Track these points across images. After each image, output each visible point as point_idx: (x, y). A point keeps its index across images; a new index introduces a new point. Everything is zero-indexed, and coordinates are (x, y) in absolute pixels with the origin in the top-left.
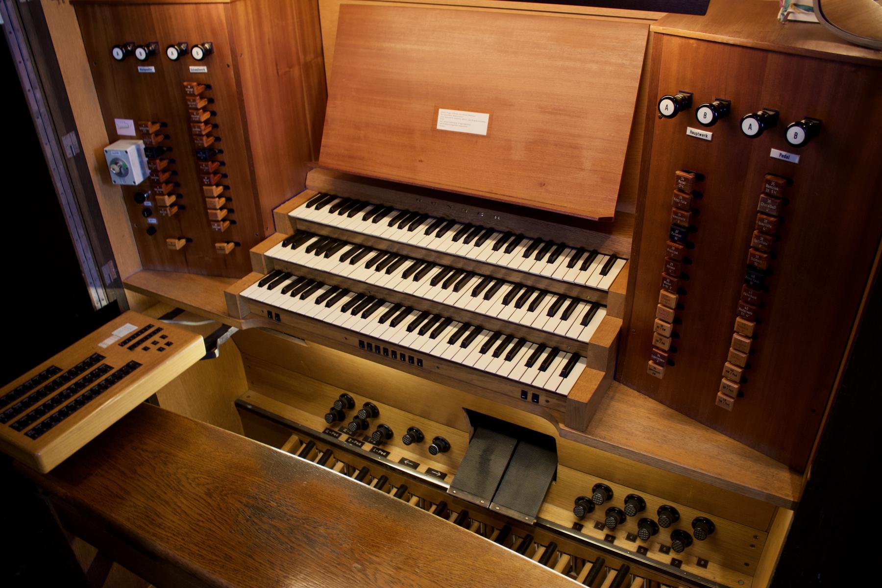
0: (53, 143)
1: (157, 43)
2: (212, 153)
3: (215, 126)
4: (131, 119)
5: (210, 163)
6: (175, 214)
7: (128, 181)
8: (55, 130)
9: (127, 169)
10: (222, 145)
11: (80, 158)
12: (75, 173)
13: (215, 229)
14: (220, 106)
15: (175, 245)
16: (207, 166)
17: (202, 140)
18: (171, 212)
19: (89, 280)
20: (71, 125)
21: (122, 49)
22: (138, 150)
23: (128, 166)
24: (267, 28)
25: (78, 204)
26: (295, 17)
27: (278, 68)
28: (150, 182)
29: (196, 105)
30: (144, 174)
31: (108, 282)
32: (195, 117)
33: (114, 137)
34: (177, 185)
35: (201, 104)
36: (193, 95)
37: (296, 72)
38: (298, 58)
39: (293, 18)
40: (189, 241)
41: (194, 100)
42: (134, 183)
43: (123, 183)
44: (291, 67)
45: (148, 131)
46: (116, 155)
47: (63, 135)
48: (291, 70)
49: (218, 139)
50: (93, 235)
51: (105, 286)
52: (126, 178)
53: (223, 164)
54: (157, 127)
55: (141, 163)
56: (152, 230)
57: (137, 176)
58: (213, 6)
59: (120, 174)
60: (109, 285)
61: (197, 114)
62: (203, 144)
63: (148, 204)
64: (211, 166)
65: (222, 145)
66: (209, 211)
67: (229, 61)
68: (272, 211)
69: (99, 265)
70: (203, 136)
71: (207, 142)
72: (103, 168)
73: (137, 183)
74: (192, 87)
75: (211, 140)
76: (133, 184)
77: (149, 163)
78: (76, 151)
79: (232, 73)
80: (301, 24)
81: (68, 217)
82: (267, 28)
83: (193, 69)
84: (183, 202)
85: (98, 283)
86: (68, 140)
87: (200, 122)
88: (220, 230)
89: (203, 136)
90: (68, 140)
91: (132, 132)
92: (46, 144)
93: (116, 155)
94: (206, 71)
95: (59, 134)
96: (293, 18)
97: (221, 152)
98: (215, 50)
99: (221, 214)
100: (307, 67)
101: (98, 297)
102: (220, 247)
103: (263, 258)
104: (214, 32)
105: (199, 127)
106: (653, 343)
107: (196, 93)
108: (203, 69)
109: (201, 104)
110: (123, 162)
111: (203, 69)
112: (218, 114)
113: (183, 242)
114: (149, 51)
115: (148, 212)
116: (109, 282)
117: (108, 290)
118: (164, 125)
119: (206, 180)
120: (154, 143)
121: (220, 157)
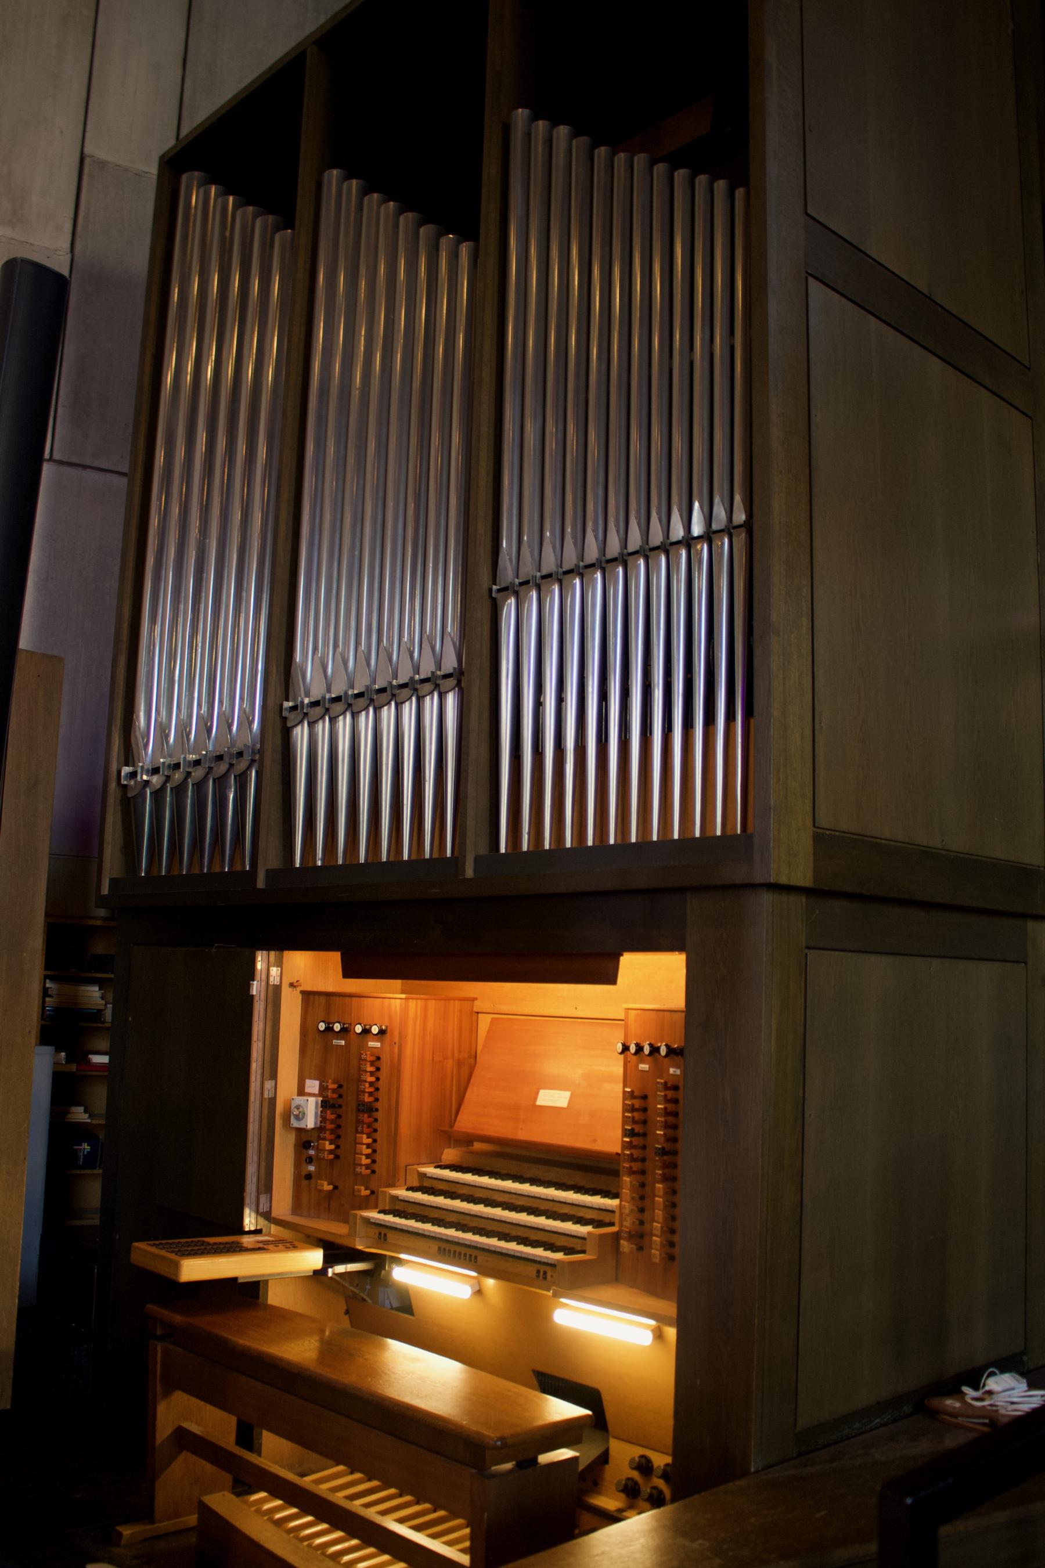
0: (259, 1082)
1: (351, 1024)
2: (371, 1109)
3: (377, 1089)
4: (317, 1080)
5: (366, 1115)
6: (331, 1160)
7: (302, 1125)
8: (263, 1074)
9: (304, 1114)
10: (378, 1105)
11: (273, 1101)
12: (265, 1111)
13: (357, 1171)
14: (384, 1074)
15: (323, 1186)
16: (363, 1117)
17: (364, 1095)
18: (327, 1157)
19: (247, 1200)
20: (274, 1076)
21: (325, 1024)
22: (317, 1103)
23: (306, 1113)
24: (430, 1023)
25: (261, 1117)
26: (456, 1022)
27: (434, 1056)
28: (319, 1129)
29: (366, 1068)
30: (316, 1123)
31: (261, 1210)
32: (363, 1077)
33: (301, 1092)
34: (338, 1137)
35: (370, 1069)
36: (365, 1060)
37: (450, 1064)
38: (453, 1054)
39: (454, 1023)
40: (336, 1188)
41: (365, 1065)
42: (307, 1126)
43: (298, 1126)
44: (445, 1058)
45: (327, 1086)
46: (300, 1102)
47: (267, 1080)
48: (445, 1061)
49: (377, 1100)
50: (263, 1164)
51: (257, 1212)
52: (302, 1122)
53: (376, 1120)
54: (335, 1086)
55: (316, 1113)
56: (309, 1176)
57: (310, 1122)
58: (394, 1000)
59: (297, 1118)
60: (262, 1213)
61: (365, 1075)
62: (364, 1098)
63: (312, 1152)
64: (365, 1117)
65: (378, 1105)
66: (357, 1156)
67: (397, 1040)
68: (406, 1166)
69: (259, 1192)
70: (366, 1092)
71: (367, 1099)
72: (287, 1116)
73: (308, 1127)
74: (366, 1055)
75: (371, 1099)
76: (305, 1127)
77: (322, 1112)
78: (271, 1095)
79: (396, 1050)
80: (460, 1029)
81: (250, 1142)
82: (430, 1023)
83: (371, 1044)
84: (338, 1152)
85: (254, 1206)
86: (269, 1085)
87: (366, 1081)
88: (361, 1172)
89: (366, 1092)
90: (269, 1085)
91: (316, 1090)
92: (257, 1001)
93: (300, 1102)
94: (379, 1046)
95: (264, 1078)
96: (454, 1023)
97: (377, 1110)
98: (388, 1031)
99: (365, 1161)
100: (460, 1063)
101: (249, 1221)
102: (358, 1189)
103: (388, 1196)
104: (390, 1019)
105: (364, 1085)
106: (945, 1531)
107: (368, 1059)
108: (378, 1044)
109: (370, 1069)
110: (303, 1109)
111: (378, 1044)
112: (381, 1080)
113: (331, 1187)
114: (344, 1027)
115: (310, 1160)
116: (262, 1211)
117: (259, 1217)
118: (341, 1086)
119: (360, 1129)
120: (329, 1097)
121: (375, 1114)
